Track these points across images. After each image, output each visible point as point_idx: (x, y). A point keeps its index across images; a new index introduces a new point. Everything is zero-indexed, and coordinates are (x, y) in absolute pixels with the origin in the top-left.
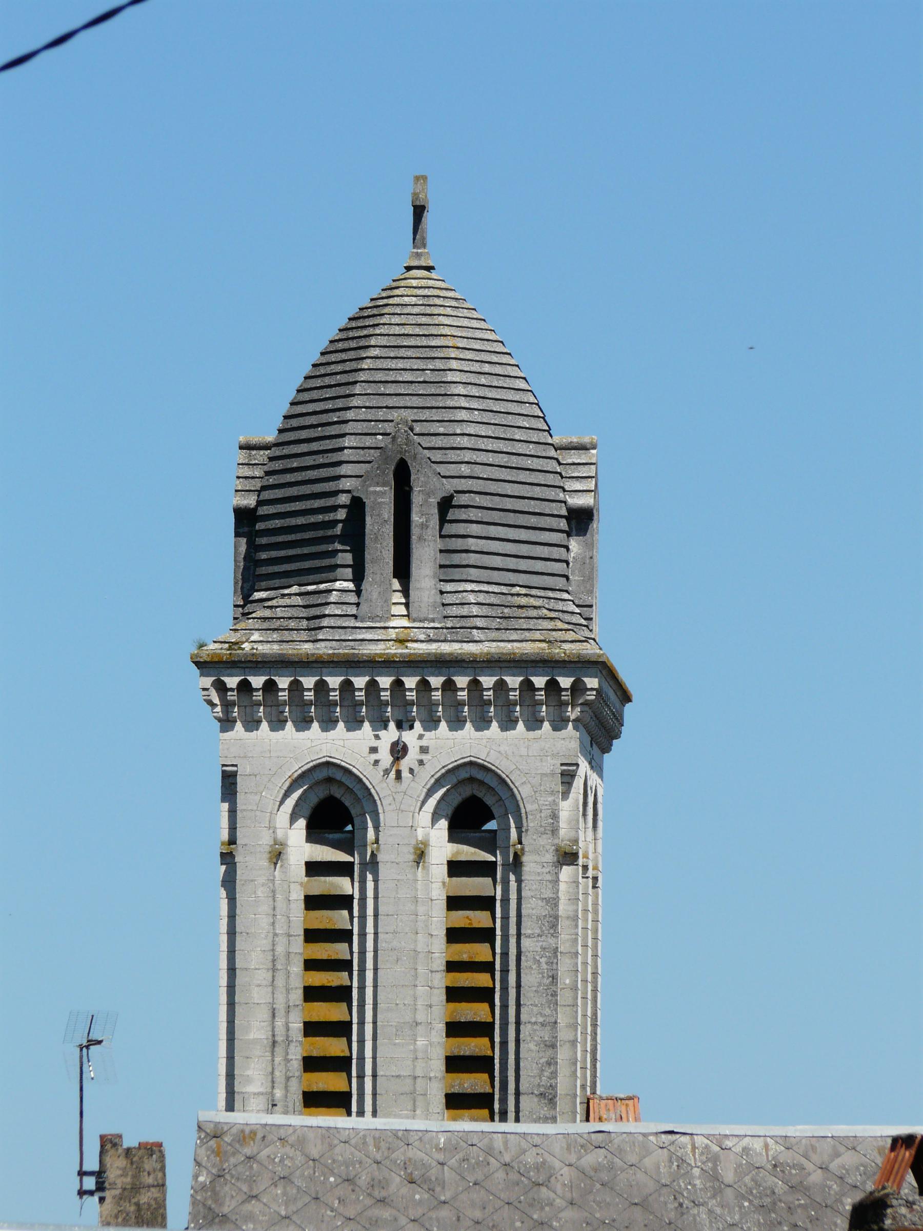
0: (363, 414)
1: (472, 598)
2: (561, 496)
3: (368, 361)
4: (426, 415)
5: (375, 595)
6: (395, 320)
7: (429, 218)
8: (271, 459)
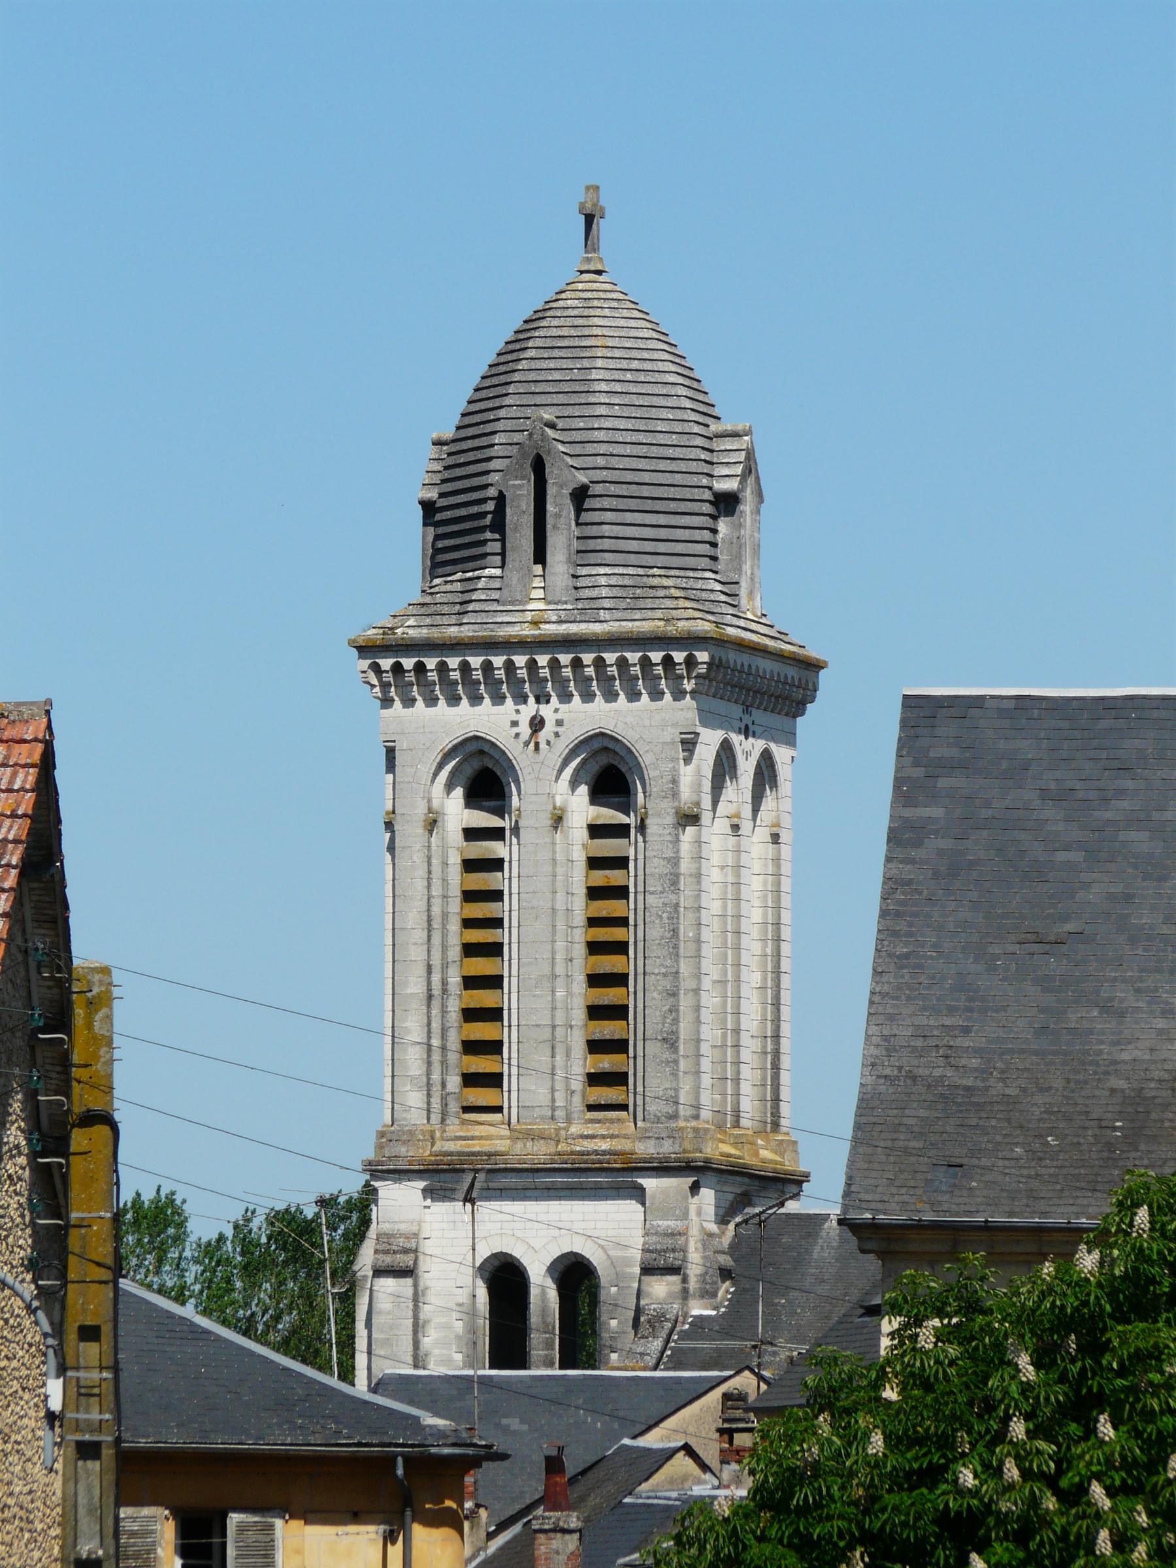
0: (513, 412)
1: (603, 581)
2: (705, 481)
4: (569, 411)
6: (555, 322)
7: (603, 227)
8: (449, 454)
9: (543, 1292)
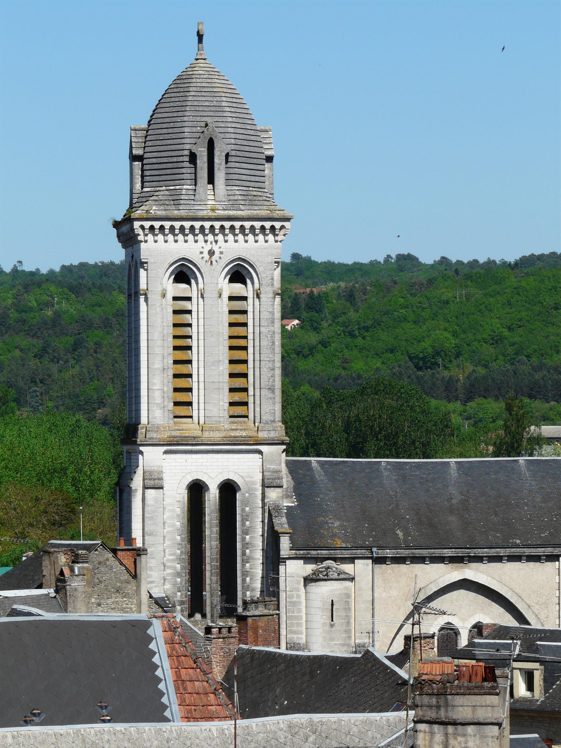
0: (191, 118)
3: (191, 97)
5: (201, 191)
9: (212, 496)
